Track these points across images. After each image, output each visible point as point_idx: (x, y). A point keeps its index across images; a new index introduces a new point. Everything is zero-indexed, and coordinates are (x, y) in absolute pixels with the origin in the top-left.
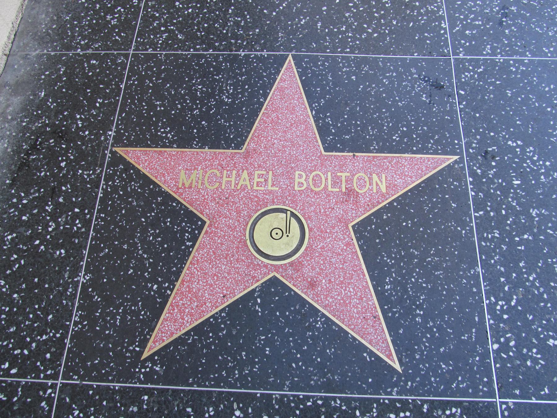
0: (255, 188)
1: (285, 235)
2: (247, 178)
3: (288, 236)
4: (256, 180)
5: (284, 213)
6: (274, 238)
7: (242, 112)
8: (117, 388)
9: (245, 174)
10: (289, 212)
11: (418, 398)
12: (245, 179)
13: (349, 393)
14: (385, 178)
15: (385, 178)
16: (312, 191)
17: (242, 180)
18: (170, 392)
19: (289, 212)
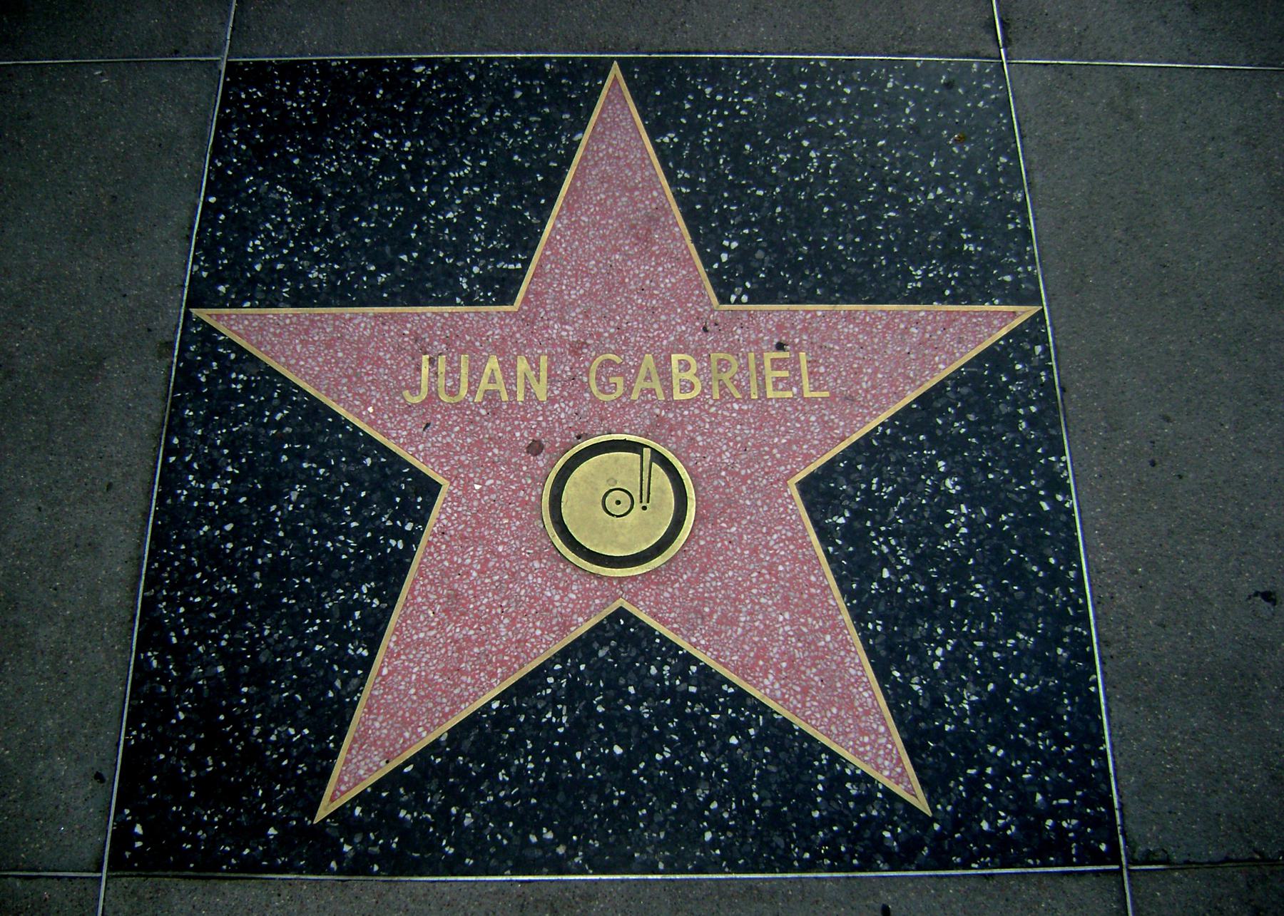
0: (678, 396)
1: (637, 506)
2: (499, 375)
3: (644, 508)
4: (771, 375)
5: (635, 451)
6: (614, 507)
7: (729, 201)
8: (1092, 689)
9: (493, 363)
10: (647, 452)
11: (1030, 870)
12: (649, 372)
13: (899, 806)
14: (875, 361)
15: (875, 361)
16: (618, 399)
17: (485, 380)
18: (135, 703)
19: (647, 452)
